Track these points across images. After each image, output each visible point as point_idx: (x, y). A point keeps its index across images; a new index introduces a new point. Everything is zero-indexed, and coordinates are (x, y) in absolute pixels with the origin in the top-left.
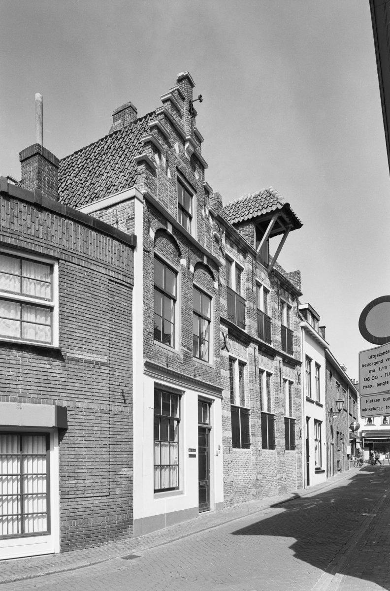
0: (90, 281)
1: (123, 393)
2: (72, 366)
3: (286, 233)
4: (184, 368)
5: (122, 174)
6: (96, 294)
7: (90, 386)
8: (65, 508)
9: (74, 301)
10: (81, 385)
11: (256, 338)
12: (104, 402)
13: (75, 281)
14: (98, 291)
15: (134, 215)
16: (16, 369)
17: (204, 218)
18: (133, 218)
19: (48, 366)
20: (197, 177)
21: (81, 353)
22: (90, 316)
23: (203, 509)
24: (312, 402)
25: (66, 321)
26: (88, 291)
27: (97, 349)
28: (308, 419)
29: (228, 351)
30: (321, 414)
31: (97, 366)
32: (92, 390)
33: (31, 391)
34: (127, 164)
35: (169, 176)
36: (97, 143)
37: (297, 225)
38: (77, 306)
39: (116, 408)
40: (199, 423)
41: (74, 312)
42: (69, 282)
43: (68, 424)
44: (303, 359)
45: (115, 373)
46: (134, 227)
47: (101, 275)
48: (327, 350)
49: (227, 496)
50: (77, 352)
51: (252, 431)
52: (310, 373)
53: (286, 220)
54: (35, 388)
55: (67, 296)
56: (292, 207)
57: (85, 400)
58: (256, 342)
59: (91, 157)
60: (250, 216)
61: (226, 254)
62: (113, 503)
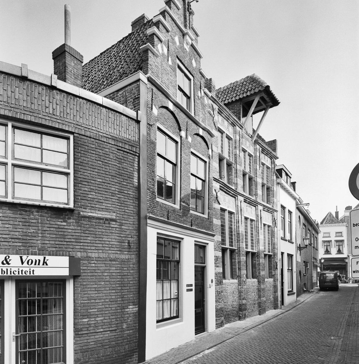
0: (101, 151)
1: (129, 243)
2: (85, 223)
3: (265, 109)
4: (182, 219)
5: (132, 64)
6: (106, 161)
7: (101, 239)
8: (78, 342)
9: (87, 168)
10: (92, 239)
11: (242, 192)
12: (113, 252)
13: (88, 151)
14: (108, 159)
15: (139, 95)
16: (35, 227)
17: (200, 97)
18: (139, 97)
19: (65, 224)
20: (194, 64)
21: (93, 211)
22: (101, 180)
23: (201, 331)
24: (286, 240)
25: (80, 185)
26: (99, 159)
27: (107, 208)
28: (282, 253)
29: (220, 204)
30: (291, 249)
31: (107, 222)
32: (103, 242)
33: (49, 245)
34: (137, 56)
35: (170, 63)
36: (116, 44)
37: (275, 102)
38: (89, 172)
39: (123, 257)
40: (195, 263)
41: (87, 177)
42: (82, 152)
43: (82, 271)
44: (279, 209)
45: (123, 227)
46: (139, 105)
47: (111, 145)
48: (297, 200)
49: (218, 319)
50: (90, 211)
51: (238, 266)
52: (284, 218)
53: (267, 100)
54: (53, 242)
55: (81, 164)
56: (271, 89)
57: (96, 251)
58: (242, 195)
59: (111, 55)
60: (237, 98)
61: (218, 127)
62: (120, 336)
